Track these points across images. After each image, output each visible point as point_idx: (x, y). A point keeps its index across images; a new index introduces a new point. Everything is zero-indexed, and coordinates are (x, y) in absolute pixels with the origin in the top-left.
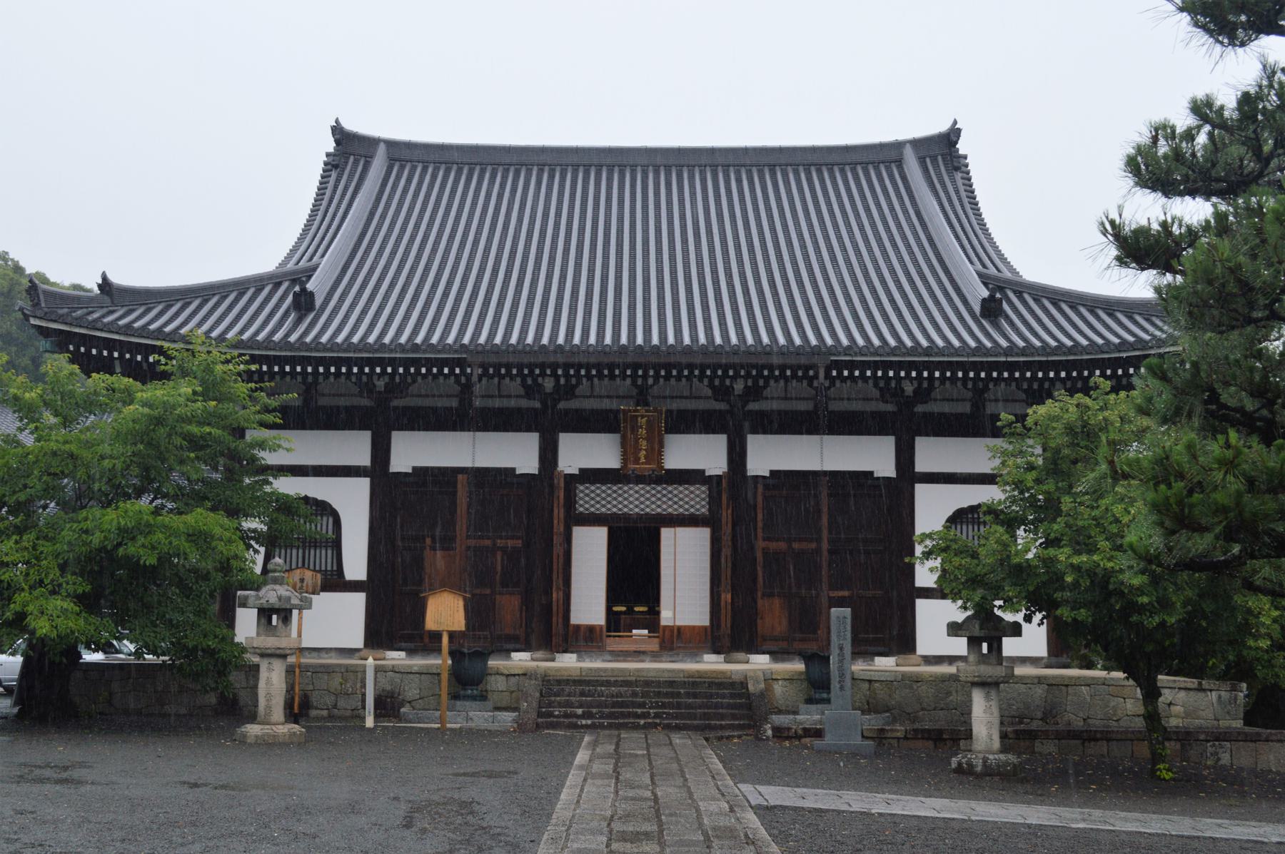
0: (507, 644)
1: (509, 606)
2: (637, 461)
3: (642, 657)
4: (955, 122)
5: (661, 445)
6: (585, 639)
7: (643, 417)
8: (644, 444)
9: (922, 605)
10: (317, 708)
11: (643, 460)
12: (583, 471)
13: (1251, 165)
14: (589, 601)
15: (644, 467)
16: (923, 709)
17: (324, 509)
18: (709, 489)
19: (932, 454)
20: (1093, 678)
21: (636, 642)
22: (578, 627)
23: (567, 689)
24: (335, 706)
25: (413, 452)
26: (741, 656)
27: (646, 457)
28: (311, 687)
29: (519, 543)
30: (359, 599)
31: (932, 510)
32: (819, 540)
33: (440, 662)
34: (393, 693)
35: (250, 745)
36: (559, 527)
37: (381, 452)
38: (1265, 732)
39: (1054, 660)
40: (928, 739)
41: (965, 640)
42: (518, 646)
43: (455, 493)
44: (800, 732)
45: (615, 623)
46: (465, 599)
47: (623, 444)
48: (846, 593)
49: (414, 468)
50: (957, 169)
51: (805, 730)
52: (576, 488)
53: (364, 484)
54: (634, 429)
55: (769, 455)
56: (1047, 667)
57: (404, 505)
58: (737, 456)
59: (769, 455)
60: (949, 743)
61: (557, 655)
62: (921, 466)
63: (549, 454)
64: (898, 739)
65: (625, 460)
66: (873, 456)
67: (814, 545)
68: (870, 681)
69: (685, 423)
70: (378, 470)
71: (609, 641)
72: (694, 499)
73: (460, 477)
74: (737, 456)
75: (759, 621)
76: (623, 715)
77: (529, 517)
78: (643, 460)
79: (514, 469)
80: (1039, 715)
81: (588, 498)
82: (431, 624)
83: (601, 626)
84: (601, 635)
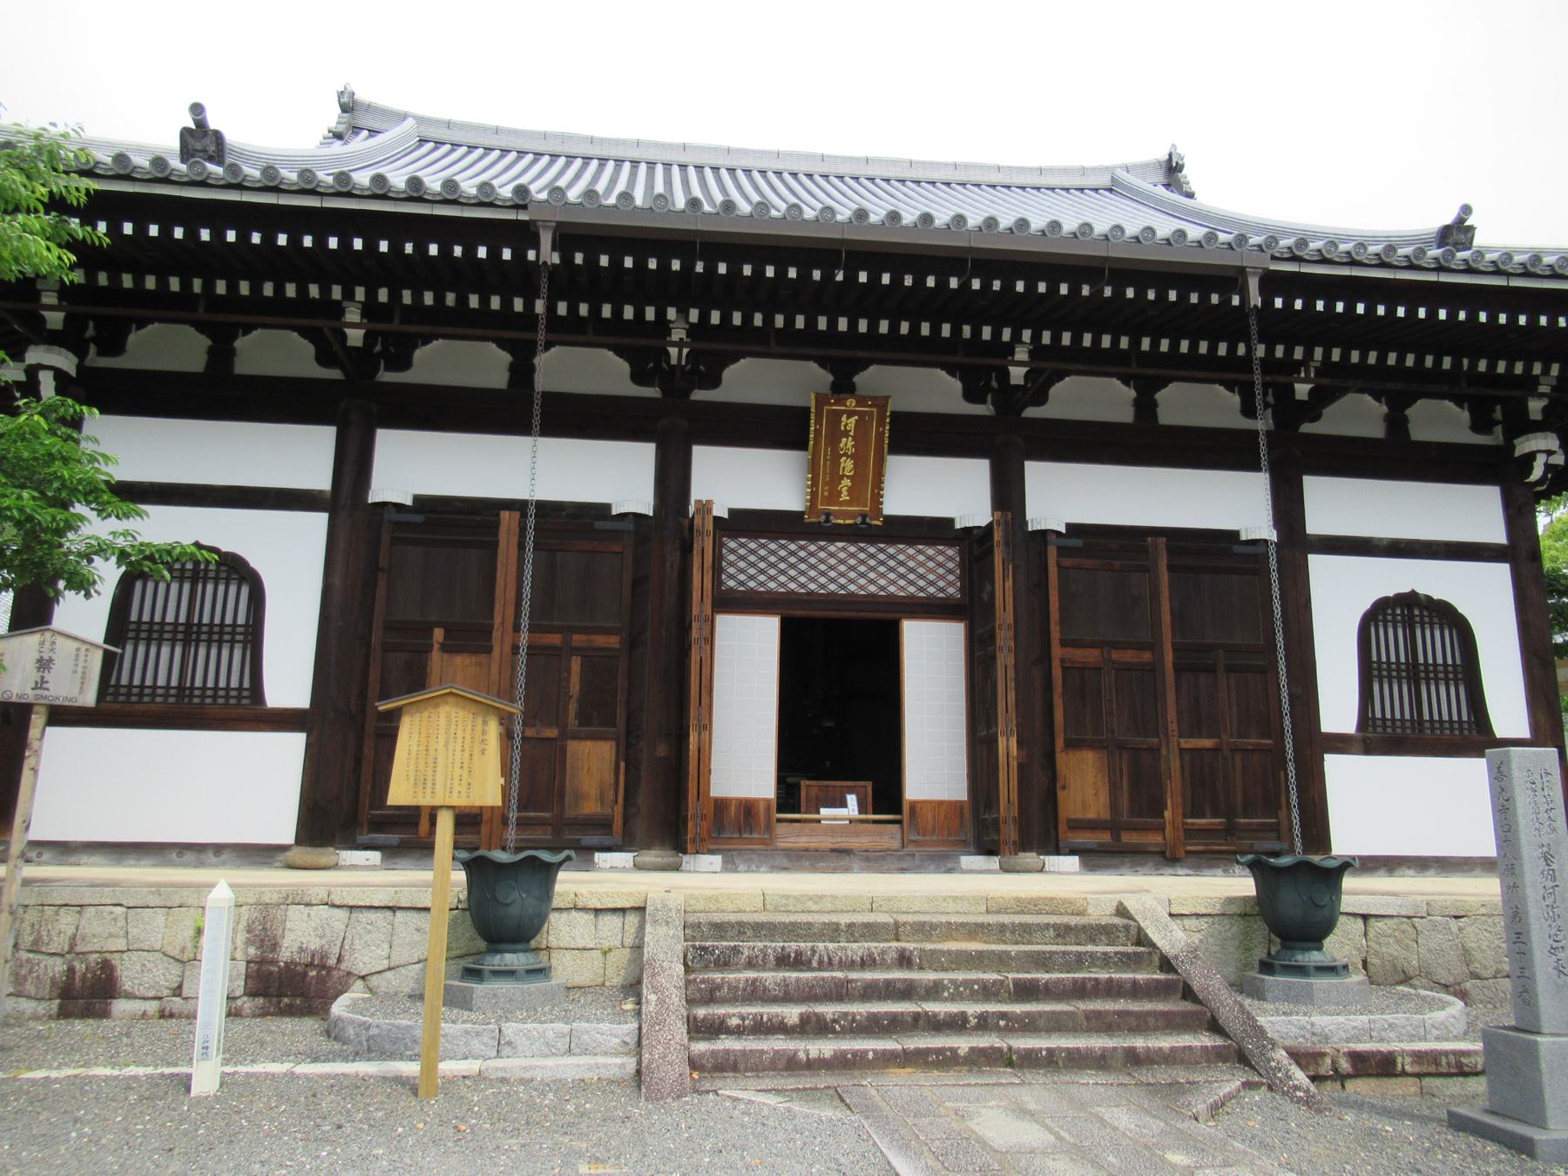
0: (585, 838)
1: (593, 764)
2: (834, 497)
3: (845, 861)
6: (739, 830)
7: (850, 414)
8: (847, 465)
9: (1336, 767)
10: (130, 996)
11: (845, 497)
14: (742, 746)
15: (845, 510)
17: (235, 569)
18: (961, 553)
19: (1332, 504)
21: (832, 831)
22: (721, 805)
26: (1030, 858)
27: (850, 490)
28: (120, 944)
29: (613, 641)
30: (293, 744)
31: (1340, 596)
32: (1154, 646)
33: (440, 880)
34: (324, 956)
37: (353, 464)
42: (607, 841)
43: (493, 546)
44: (1345, 1065)
46: (506, 720)
47: (813, 467)
48: (1207, 743)
49: (417, 499)
51: (1355, 1057)
53: (316, 524)
54: (836, 435)
55: (1063, 496)
57: (408, 592)
58: (1008, 493)
59: (1063, 496)
62: (1318, 522)
63: (672, 479)
66: (1234, 503)
67: (1146, 656)
69: (923, 435)
71: (781, 829)
72: (933, 570)
73: (505, 515)
74: (1008, 493)
75: (1060, 794)
77: (645, 582)
78: (845, 497)
82: (400, 793)
83: (768, 800)
84: (768, 818)
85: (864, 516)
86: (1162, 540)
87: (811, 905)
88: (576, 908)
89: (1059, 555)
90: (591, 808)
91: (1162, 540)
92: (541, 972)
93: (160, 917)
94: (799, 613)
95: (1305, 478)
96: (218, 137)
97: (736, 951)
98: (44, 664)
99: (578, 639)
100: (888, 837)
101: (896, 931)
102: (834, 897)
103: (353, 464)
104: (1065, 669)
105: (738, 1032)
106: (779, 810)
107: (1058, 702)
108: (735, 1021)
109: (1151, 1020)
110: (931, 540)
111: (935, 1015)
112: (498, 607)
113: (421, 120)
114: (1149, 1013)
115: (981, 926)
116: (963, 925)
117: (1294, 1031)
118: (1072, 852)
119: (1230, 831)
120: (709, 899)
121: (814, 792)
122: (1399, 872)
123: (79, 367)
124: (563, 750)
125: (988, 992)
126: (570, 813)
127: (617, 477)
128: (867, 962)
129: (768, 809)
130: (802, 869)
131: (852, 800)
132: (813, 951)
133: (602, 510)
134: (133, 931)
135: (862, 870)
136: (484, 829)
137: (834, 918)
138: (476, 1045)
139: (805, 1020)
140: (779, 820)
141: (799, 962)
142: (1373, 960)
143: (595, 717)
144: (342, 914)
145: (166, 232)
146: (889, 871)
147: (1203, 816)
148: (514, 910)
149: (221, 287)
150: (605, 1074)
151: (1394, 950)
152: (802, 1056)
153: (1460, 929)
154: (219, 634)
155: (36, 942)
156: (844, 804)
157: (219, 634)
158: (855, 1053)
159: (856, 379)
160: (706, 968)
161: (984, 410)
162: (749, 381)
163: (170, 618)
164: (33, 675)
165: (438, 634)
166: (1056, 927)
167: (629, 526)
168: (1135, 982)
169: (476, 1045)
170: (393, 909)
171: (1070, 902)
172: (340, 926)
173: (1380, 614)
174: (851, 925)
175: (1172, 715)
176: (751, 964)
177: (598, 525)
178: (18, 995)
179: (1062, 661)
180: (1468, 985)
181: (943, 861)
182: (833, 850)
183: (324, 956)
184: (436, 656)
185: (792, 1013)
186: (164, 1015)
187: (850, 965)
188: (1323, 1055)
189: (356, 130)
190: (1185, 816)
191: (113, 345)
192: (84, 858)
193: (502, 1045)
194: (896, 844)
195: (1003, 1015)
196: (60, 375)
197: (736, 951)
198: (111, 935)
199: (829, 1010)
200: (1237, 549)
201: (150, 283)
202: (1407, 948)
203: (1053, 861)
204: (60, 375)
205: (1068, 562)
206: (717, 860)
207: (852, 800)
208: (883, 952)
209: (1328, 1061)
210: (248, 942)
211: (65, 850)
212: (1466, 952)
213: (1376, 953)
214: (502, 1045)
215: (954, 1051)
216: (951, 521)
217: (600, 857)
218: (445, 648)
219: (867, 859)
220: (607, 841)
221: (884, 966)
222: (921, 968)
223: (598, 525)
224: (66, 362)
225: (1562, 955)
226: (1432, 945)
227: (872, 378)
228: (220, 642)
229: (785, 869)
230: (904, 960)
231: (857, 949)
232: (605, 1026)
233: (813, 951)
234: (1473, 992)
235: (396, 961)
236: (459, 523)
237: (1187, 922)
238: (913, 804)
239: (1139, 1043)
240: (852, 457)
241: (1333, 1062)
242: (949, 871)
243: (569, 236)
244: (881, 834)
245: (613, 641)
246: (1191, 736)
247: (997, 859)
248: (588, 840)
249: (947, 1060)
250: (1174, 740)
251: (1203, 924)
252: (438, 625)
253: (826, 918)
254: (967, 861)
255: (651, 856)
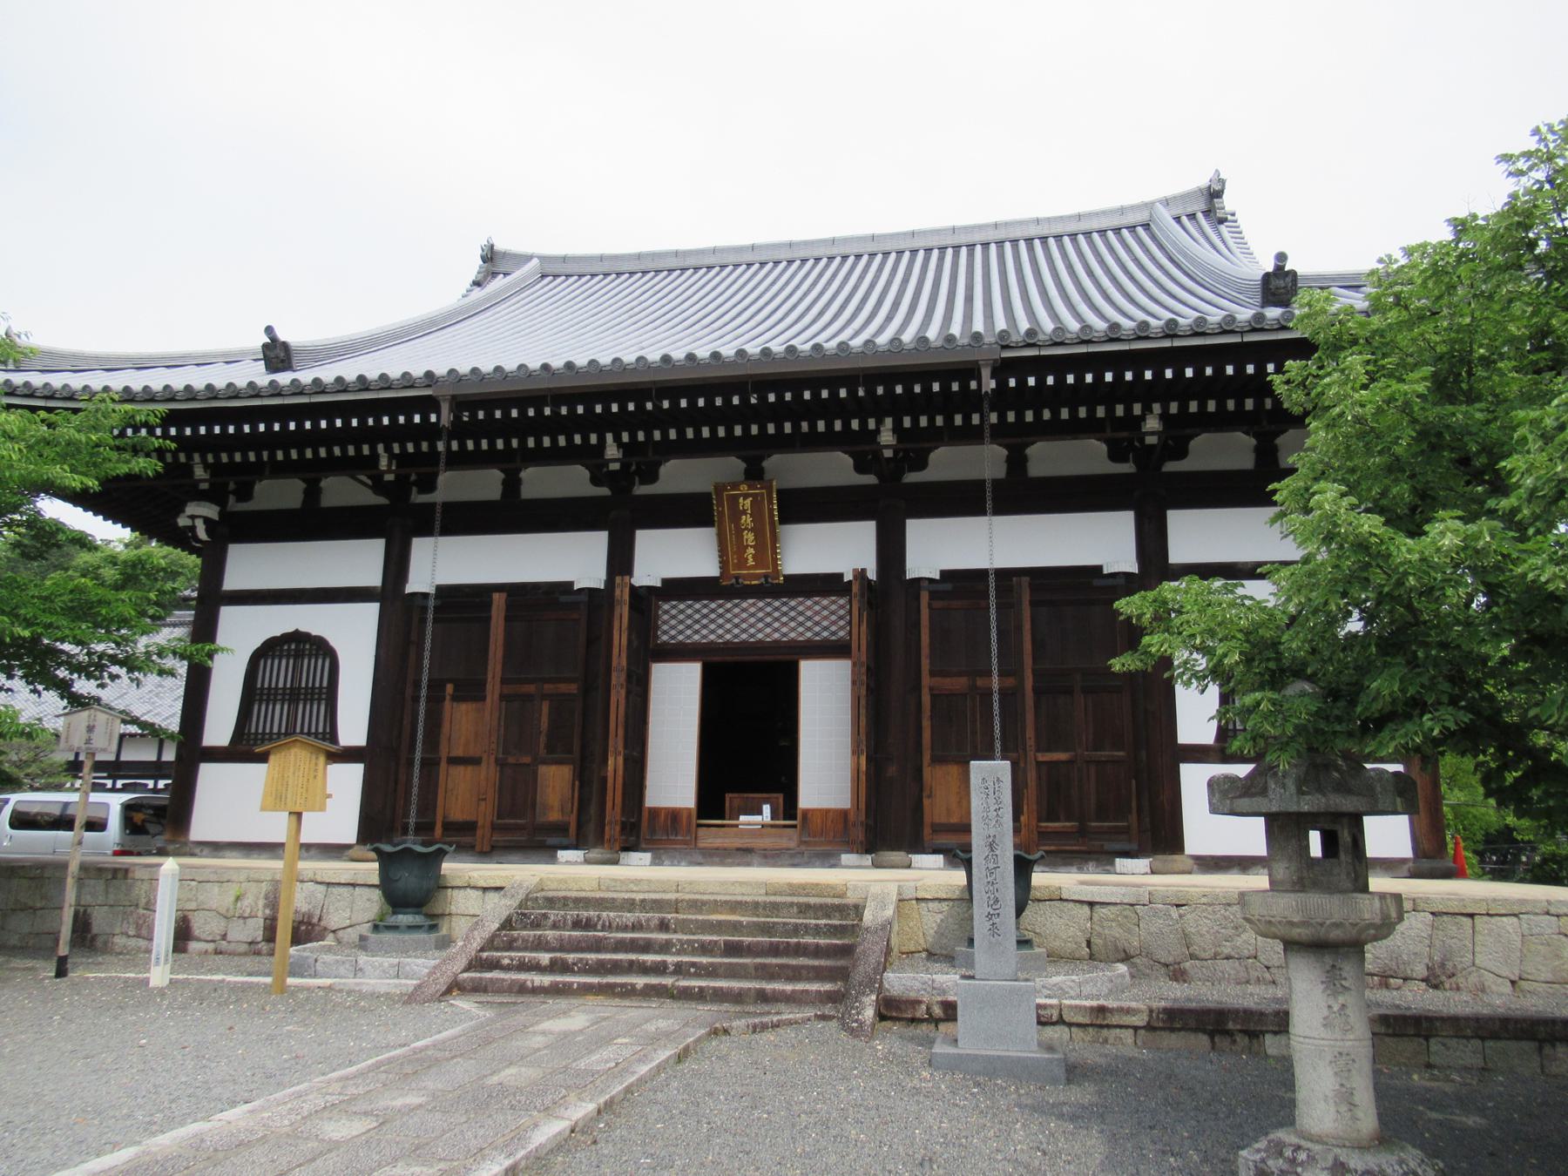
2: (742, 563)
3: (749, 858)
4: (1281, 257)
5: (775, 538)
7: (746, 496)
8: (749, 537)
10: (199, 940)
11: (751, 562)
12: (667, 582)
13: (1410, 618)
14: (673, 777)
15: (752, 572)
16: (1193, 957)
20: (1522, 902)
21: (752, 833)
22: (655, 812)
23: (553, 915)
24: (224, 937)
25: (441, 563)
27: (754, 557)
28: (193, 906)
29: (573, 688)
34: (310, 916)
35: (161, 992)
36: (620, 659)
37: (396, 566)
38: (862, 730)
39: (1426, 864)
40: (1196, 1030)
41: (1260, 822)
42: (565, 841)
44: (938, 1011)
45: (712, 801)
48: (1063, 756)
50: (1222, 221)
52: (659, 607)
53: (371, 611)
54: (736, 514)
55: (939, 547)
56: (1415, 875)
58: (891, 549)
59: (939, 547)
60: (1242, 1041)
61: (623, 855)
62: (1179, 553)
64: (1136, 1028)
65: (724, 564)
66: (1101, 541)
68: (1091, 904)
70: (390, 594)
71: (702, 831)
73: (496, 596)
74: (891, 549)
75: (926, 802)
76: (616, 968)
78: (751, 562)
79: (571, 583)
80: (1420, 970)
81: (677, 623)
83: (689, 810)
84: (689, 823)
85: (766, 576)
86: (1026, 580)
87: (632, 886)
88: (469, 887)
89: (931, 598)
90: (554, 816)
91: (1026, 580)
92: (433, 928)
93: (216, 889)
94: (716, 659)
95: (909, 522)
96: (285, 345)
97: (545, 916)
98: (90, 729)
99: (548, 688)
100: (789, 839)
101: (658, 905)
102: (649, 881)
103: (396, 566)
104: (934, 697)
105: (508, 968)
106: (699, 817)
107: (926, 723)
108: (506, 961)
109: (804, 972)
110: (824, 593)
111: (644, 962)
112: (490, 668)
113: (543, 259)
114: (803, 967)
115: (740, 903)
116: (726, 902)
117: (917, 985)
118: (935, 852)
119: (1082, 832)
120: (560, 881)
121: (736, 803)
122: (1255, 870)
123: (220, 514)
124: (535, 773)
125: (705, 949)
126: (540, 819)
127: (576, 560)
128: (637, 927)
129: (689, 816)
130: (713, 864)
131: (766, 809)
132: (599, 917)
133: (566, 587)
134: (201, 898)
135: (760, 865)
136: (479, 832)
137: (633, 896)
138: (342, 970)
139: (553, 962)
140: (699, 826)
141: (588, 925)
142: (1096, 941)
143: (557, 749)
144: (322, 888)
145: (239, 429)
146: (782, 866)
147: (1058, 820)
148: (401, 885)
149: (280, 455)
150: (404, 990)
151: (1117, 932)
152: (529, 984)
153: (1181, 916)
154: (311, 695)
155: (148, 903)
156: (760, 812)
157: (311, 695)
158: (564, 984)
159: (765, 464)
160: (525, 928)
161: (1127, 468)
162: (678, 476)
163: (281, 685)
164: (85, 736)
165: (450, 688)
166: (799, 905)
167: (584, 598)
168: (817, 945)
169: (342, 970)
170: (354, 885)
171: (832, 887)
172: (320, 896)
173: (269, 649)
174: (643, 901)
175: (1030, 733)
176: (555, 926)
177: (563, 599)
178: (138, 936)
179: (931, 689)
180: (1187, 965)
181: (828, 859)
182: (738, 849)
183: (310, 916)
184: (447, 704)
185: (545, 958)
186: (218, 952)
187: (625, 928)
188: (920, 1002)
189: (494, 274)
190: (1039, 820)
191: (245, 493)
192: (228, 853)
193: (357, 971)
194: (792, 844)
195: (693, 964)
196: (207, 521)
197: (545, 916)
198: (189, 900)
199: (571, 957)
200: (1097, 582)
201: (238, 457)
202: (1129, 931)
203: (919, 859)
204: (207, 521)
205: (938, 604)
206: (647, 856)
207: (766, 809)
208: (648, 920)
209: (924, 1007)
210: (266, 906)
211: (217, 848)
212: (1186, 935)
213: (1099, 935)
214: (357, 971)
215: (633, 985)
216: (1100, 568)
217: (561, 853)
218: (455, 698)
219: (765, 857)
220: (565, 841)
221: (649, 929)
222: (675, 932)
223: (563, 599)
224: (211, 511)
225: (997, 921)
226: (1153, 929)
227: (775, 463)
228: (312, 701)
229: (700, 864)
230: (663, 926)
231: (629, 917)
232: (420, 961)
233: (599, 917)
234: (1192, 972)
235: (354, 921)
236: (463, 602)
237: (931, 905)
238: (806, 812)
239: (769, 986)
240: (752, 530)
241: (928, 1009)
242: (832, 866)
243: (461, 403)
244: (781, 836)
245: (573, 688)
246: (1049, 750)
247: (869, 857)
248: (551, 841)
249: (628, 992)
250: (1031, 754)
251: (945, 906)
252: (450, 681)
253: (627, 896)
254: (846, 858)
255: (595, 853)
